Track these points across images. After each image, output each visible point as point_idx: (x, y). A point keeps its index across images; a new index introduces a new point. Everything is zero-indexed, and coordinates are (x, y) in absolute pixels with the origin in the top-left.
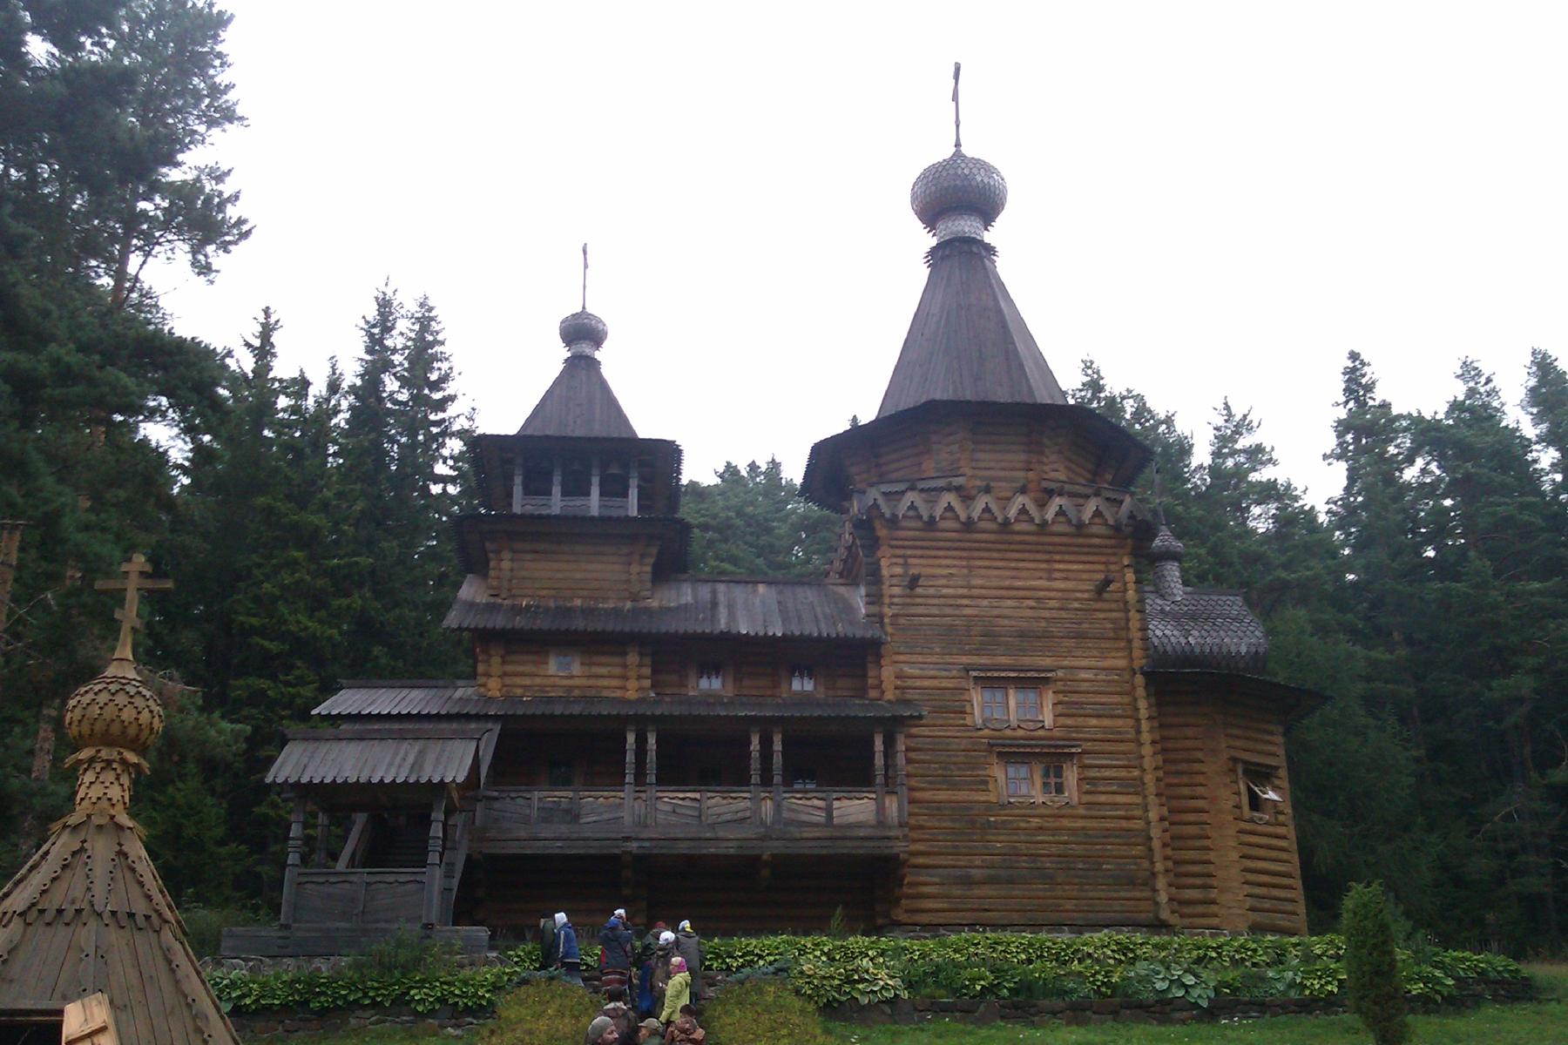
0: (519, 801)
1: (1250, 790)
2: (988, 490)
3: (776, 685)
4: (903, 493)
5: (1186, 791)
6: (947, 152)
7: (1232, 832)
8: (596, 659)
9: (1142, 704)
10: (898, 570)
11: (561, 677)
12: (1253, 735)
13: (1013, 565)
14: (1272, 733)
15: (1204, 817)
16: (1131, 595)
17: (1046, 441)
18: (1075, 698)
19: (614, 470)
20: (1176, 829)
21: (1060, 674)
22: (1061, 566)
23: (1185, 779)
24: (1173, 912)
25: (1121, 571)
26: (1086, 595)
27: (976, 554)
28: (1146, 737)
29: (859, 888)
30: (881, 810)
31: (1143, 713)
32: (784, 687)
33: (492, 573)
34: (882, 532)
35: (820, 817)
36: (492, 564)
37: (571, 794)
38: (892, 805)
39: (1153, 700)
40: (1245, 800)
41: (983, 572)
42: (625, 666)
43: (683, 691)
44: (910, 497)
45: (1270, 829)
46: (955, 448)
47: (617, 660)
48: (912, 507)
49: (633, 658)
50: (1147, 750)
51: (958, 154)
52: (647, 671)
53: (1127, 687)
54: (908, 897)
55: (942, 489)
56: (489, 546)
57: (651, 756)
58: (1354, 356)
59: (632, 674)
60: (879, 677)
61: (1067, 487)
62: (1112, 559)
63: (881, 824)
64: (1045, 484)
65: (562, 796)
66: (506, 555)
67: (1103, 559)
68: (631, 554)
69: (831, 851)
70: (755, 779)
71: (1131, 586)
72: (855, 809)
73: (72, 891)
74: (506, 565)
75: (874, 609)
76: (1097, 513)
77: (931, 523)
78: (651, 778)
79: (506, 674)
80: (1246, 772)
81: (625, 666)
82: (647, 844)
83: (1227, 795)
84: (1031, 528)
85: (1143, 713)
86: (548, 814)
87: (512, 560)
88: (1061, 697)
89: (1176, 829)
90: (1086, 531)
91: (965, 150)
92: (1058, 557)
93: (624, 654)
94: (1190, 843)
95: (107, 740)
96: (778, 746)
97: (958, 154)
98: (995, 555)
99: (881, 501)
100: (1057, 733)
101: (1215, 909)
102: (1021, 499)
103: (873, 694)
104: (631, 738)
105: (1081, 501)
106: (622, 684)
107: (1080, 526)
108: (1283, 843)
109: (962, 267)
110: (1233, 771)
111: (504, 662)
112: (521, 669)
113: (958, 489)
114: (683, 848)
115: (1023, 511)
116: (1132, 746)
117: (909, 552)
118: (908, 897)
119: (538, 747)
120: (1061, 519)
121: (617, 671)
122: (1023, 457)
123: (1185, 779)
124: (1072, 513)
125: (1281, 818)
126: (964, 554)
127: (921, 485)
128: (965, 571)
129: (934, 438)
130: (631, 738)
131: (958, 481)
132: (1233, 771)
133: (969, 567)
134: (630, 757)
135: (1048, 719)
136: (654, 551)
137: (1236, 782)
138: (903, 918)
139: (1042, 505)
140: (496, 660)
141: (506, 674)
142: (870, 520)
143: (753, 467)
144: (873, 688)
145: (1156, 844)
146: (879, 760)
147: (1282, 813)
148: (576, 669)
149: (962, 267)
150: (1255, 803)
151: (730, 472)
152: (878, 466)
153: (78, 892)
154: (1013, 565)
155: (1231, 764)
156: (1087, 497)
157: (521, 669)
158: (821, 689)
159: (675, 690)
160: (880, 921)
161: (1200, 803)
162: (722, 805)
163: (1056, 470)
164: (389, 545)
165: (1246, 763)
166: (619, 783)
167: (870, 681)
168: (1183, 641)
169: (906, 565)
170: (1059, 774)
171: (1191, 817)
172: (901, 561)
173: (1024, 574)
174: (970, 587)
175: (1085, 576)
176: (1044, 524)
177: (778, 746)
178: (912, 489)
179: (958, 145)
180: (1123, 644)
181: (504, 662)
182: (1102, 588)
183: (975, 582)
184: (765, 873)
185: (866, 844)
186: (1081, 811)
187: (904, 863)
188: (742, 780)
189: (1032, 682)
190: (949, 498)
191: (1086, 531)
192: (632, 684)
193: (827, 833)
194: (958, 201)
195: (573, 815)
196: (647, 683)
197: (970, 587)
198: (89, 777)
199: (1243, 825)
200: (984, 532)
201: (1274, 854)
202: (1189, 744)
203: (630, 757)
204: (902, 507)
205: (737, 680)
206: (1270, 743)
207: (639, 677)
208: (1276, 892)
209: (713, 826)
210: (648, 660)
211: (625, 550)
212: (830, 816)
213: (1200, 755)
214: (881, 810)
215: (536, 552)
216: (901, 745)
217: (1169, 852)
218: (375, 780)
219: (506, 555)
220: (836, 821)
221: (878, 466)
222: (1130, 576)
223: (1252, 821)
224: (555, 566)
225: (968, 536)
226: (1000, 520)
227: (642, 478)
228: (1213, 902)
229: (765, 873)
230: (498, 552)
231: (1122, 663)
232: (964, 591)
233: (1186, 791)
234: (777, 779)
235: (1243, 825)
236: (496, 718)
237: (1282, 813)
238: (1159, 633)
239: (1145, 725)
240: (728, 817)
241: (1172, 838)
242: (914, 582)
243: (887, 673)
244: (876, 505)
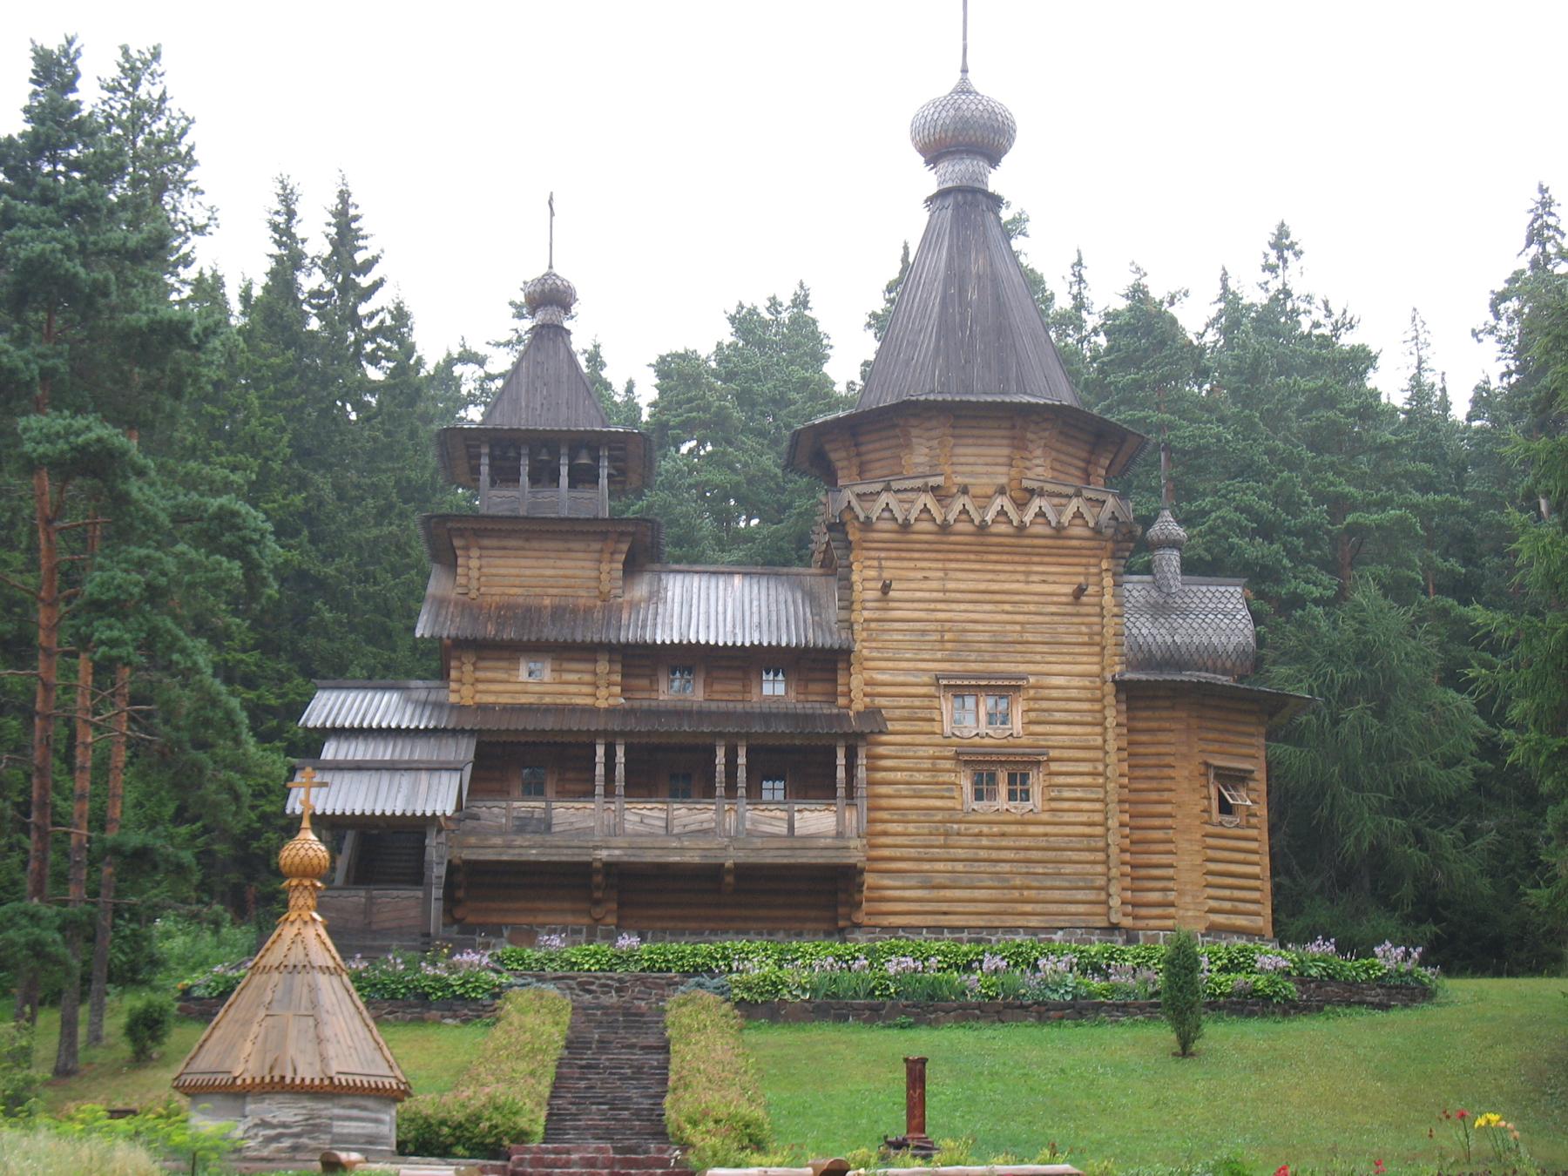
0: (496, 810)
1: (1221, 796)
2: (964, 490)
3: (746, 690)
4: (878, 493)
5: (1154, 796)
6: (542, 270)
7: (1198, 836)
8: (566, 665)
9: (1110, 713)
10: (872, 573)
11: (532, 683)
12: (1232, 738)
13: (990, 567)
14: (1252, 735)
15: (1169, 822)
16: (1108, 599)
17: (1029, 435)
18: (1045, 705)
19: (584, 460)
20: (1138, 835)
21: (1032, 680)
22: (1040, 569)
23: (1154, 784)
24: (1125, 915)
25: (1099, 574)
26: (1063, 599)
27: (952, 556)
28: (1112, 746)
29: (820, 894)
30: (840, 821)
31: (1111, 722)
32: (755, 690)
33: (460, 570)
34: (854, 535)
35: (782, 829)
36: (460, 561)
37: (543, 805)
38: (851, 816)
39: (1123, 707)
40: (1215, 804)
41: (960, 575)
42: (595, 674)
43: (654, 695)
44: (885, 498)
45: (1240, 832)
46: (935, 443)
47: (589, 666)
48: (887, 508)
49: (602, 667)
50: (1112, 758)
51: (964, 89)
52: (617, 678)
53: (1098, 694)
54: (869, 900)
55: (919, 490)
56: (457, 542)
57: (620, 770)
58: (1543, 190)
59: (602, 682)
60: (848, 684)
61: (1048, 487)
62: (1092, 561)
63: (839, 835)
64: (1026, 483)
65: (536, 805)
66: (475, 553)
67: (1084, 561)
68: (601, 551)
69: (792, 861)
70: (720, 791)
71: (1109, 591)
72: (816, 820)
73: (296, 956)
74: (474, 563)
75: (843, 615)
76: (1078, 515)
77: (906, 527)
78: (620, 790)
79: (477, 680)
80: (1217, 776)
81: (595, 674)
82: (617, 852)
83: (1190, 800)
84: (1010, 530)
85: (1111, 722)
86: (522, 825)
87: (480, 557)
88: (1032, 705)
89: (1138, 835)
90: (1064, 533)
91: (977, 81)
92: (1036, 559)
93: (596, 661)
94: (1154, 847)
95: (305, 875)
96: (742, 760)
97: (964, 89)
98: (972, 557)
99: (854, 503)
100: (1025, 741)
101: (1172, 910)
102: (999, 502)
103: (842, 701)
104: (600, 751)
105: (1063, 501)
106: (589, 691)
107: (1059, 528)
108: (1253, 845)
109: (968, 213)
110: (1205, 775)
111: (476, 669)
112: (490, 675)
113: (934, 489)
114: (650, 857)
115: (1002, 512)
116: (1100, 754)
117: (883, 554)
118: (869, 900)
119: (511, 756)
120: (1040, 520)
121: (588, 678)
122: (1006, 451)
123: (1154, 784)
124: (1051, 516)
125: (1253, 821)
126: (940, 556)
127: (895, 486)
128: (941, 574)
129: (914, 432)
130: (600, 751)
131: (933, 481)
132: (1205, 775)
133: (944, 570)
134: (600, 770)
135: (1017, 723)
136: (625, 547)
137: (1207, 786)
138: (866, 920)
139: (1021, 505)
140: (468, 668)
141: (477, 680)
142: (843, 524)
143: (774, 304)
144: (844, 695)
145: (1114, 850)
146: (841, 773)
147: (1255, 815)
148: (547, 675)
149: (968, 213)
150: (1225, 808)
151: (745, 322)
152: (859, 455)
153: (301, 956)
154: (990, 567)
155: (1203, 769)
156: (1069, 497)
157: (490, 675)
158: (792, 694)
159: (645, 695)
160: (841, 923)
161: (1167, 808)
162: (690, 815)
163: (1039, 469)
164: (322, 482)
165: (1217, 768)
166: (589, 794)
167: (840, 689)
168: (1169, 640)
169: (880, 568)
170: (1025, 777)
171: (1157, 822)
172: (875, 563)
173: (1002, 577)
174: (945, 591)
175: (1063, 579)
176: (1022, 527)
177: (742, 760)
178: (888, 489)
179: (965, 71)
180: (1097, 649)
181: (476, 669)
182: (1080, 592)
183: (951, 585)
184: (729, 879)
185: (825, 853)
186: (1045, 817)
187: (862, 871)
188: (708, 792)
189: (1006, 688)
190: (927, 499)
191: (1064, 533)
192: (602, 692)
193: (787, 844)
194: (965, 140)
195: (546, 825)
196: (618, 689)
197: (945, 591)
198: (297, 894)
199: (1209, 829)
200: (960, 534)
201: (1240, 856)
202: (1162, 749)
203: (600, 770)
204: (876, 509)
205: (708, 684)
206: (1252, 745)
207: (609, 684)
208: (1237, 894)
209: (679, 836)
210: (618, 667)
211: (597, 546)
212: (791, 827)
213: (1168, 760)
214: (412, 965)
215: (505, 548)
216: (862, 753)
217: (1127, 857)
218: (378, 813)
219: (475, 553)
220: (797, 832)
221: (859, 455)
222: (1108, 580)
223: (1221, 824)
224: (523, 562)
225: (945, 539)
226: (977, 522)
227: (611, 459)
228: (1172, 905)
229: (729, 879)
230: (467, 548)
231: (1095, 669)
232: (940, 595)
233: (1154, 796)
234: (742, 792)
235: (1209, 829)
236: (472, 732)
237: (1255, 815)
238: (1145, 631)
239: (1110, 735)
240: (693, 827)
241: (1132, 842)
242: (886, 588)
243: (856, 681)
244: (849, 507)
